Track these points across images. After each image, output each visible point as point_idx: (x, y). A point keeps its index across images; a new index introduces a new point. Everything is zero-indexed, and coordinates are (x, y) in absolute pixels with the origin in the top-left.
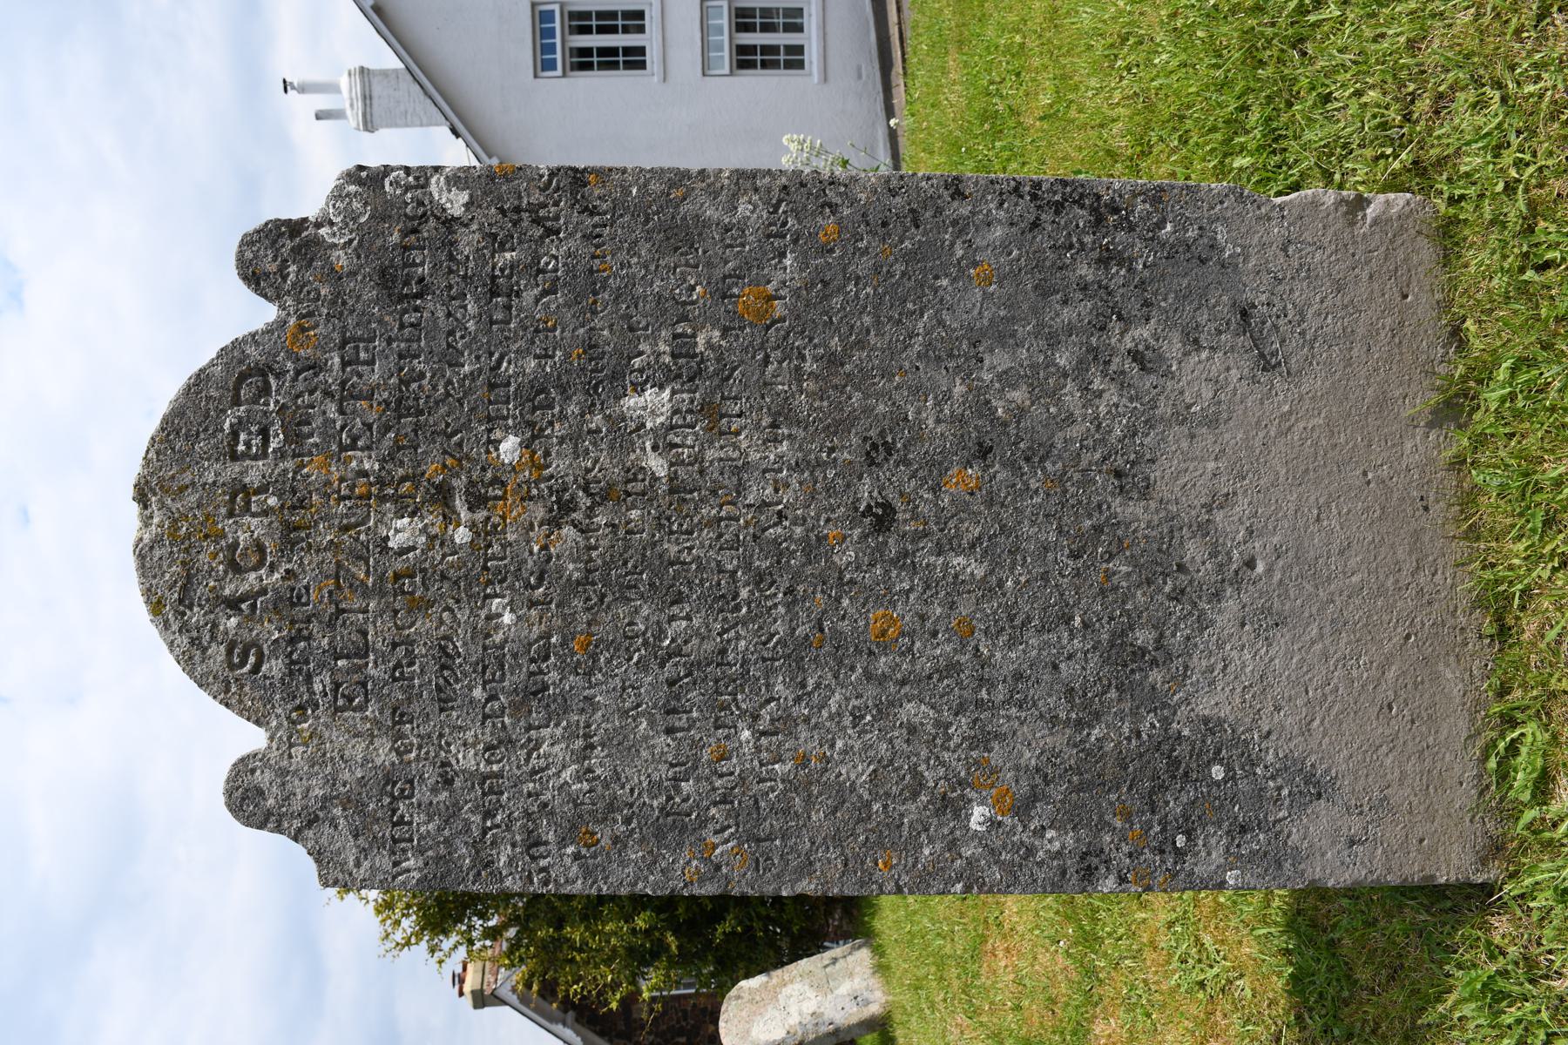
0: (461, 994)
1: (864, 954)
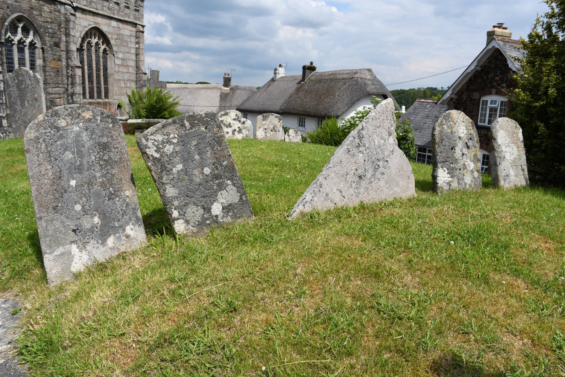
0: (494, 27)
1: (524, 183)
